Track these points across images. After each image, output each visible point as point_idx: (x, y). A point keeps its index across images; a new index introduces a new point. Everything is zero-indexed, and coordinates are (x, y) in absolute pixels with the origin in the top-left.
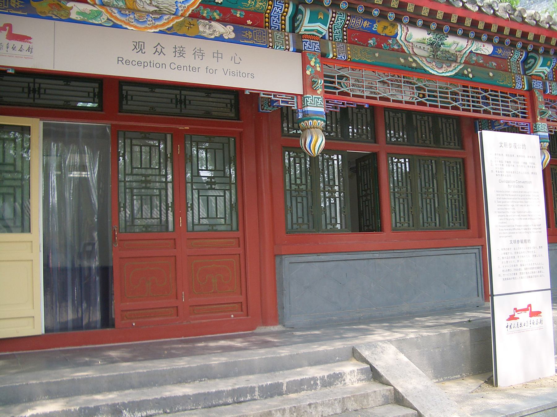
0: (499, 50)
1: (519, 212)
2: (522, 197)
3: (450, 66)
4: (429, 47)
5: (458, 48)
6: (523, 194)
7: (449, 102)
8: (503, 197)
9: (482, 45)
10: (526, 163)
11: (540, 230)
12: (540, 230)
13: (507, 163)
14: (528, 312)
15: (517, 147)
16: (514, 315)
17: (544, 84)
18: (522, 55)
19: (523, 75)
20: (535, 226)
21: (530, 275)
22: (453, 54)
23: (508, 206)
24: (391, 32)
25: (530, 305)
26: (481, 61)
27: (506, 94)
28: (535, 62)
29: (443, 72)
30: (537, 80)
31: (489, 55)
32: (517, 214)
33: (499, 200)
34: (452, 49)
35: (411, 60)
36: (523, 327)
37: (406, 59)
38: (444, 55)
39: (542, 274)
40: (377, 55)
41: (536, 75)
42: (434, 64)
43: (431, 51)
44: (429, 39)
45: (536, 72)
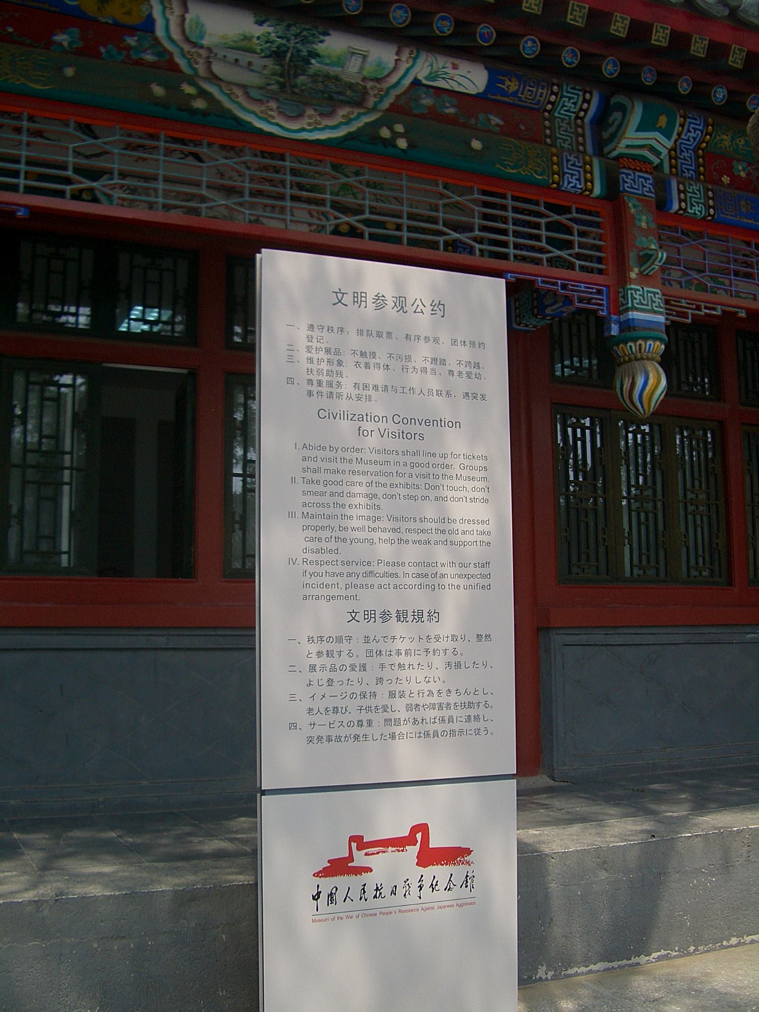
0: (508, 83)
1: (396, 519)
2: (417, 470)
3: (331, 114)
4: (269, 62)
5: (368, 70)
6: (420, 459)
7: (369, 227)
8: (332, 466)
9: (449, 65)
10: (443, 362)
11: (485, 582)
12: (485, 582)
13: (358, 358)
14: (413, 851)
15: (410, 308)
16: (351, 858)
17: (661, 185)
18: (588, 102)
19: (595, 154)
20: (462, 565)
21: (432, 728)
22: (350, 86)
23: (351, 495)
24: (129, 13)
25: (423, 828)
26: (451, 111)
27: (537, 204)
28: (623, 119)
29: (303, 130)
30: (635, 169)
31: (477, 97)
32: (385, 524)
33: (309, 476)
34: (352, 70)
35: (189, 89)
36: (389, 900)
37: (172, 89)
38: (321, 87)
39: (481, 725)
40: (69, 72)
41: (634, 158)
42: (273, 105)
43: (274, 74)
44: (263, 39)
45: (628, 147)
